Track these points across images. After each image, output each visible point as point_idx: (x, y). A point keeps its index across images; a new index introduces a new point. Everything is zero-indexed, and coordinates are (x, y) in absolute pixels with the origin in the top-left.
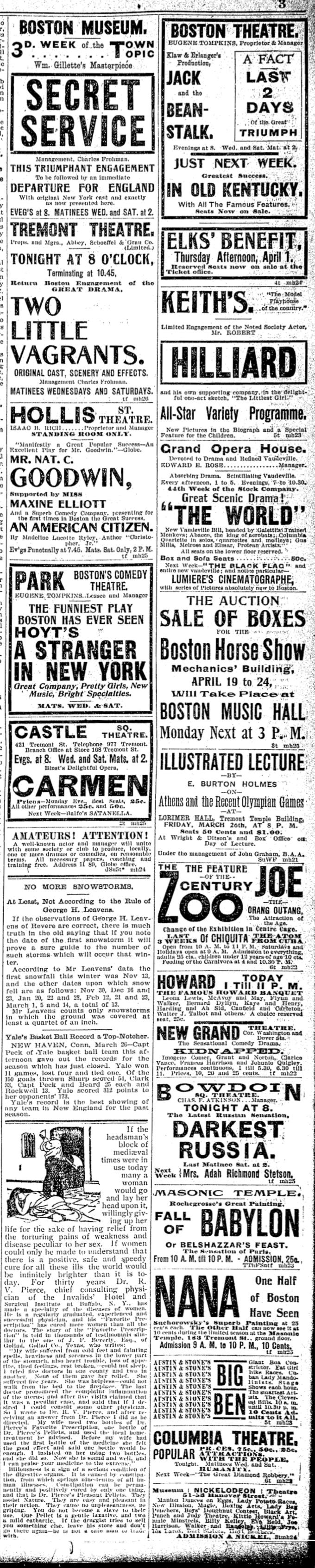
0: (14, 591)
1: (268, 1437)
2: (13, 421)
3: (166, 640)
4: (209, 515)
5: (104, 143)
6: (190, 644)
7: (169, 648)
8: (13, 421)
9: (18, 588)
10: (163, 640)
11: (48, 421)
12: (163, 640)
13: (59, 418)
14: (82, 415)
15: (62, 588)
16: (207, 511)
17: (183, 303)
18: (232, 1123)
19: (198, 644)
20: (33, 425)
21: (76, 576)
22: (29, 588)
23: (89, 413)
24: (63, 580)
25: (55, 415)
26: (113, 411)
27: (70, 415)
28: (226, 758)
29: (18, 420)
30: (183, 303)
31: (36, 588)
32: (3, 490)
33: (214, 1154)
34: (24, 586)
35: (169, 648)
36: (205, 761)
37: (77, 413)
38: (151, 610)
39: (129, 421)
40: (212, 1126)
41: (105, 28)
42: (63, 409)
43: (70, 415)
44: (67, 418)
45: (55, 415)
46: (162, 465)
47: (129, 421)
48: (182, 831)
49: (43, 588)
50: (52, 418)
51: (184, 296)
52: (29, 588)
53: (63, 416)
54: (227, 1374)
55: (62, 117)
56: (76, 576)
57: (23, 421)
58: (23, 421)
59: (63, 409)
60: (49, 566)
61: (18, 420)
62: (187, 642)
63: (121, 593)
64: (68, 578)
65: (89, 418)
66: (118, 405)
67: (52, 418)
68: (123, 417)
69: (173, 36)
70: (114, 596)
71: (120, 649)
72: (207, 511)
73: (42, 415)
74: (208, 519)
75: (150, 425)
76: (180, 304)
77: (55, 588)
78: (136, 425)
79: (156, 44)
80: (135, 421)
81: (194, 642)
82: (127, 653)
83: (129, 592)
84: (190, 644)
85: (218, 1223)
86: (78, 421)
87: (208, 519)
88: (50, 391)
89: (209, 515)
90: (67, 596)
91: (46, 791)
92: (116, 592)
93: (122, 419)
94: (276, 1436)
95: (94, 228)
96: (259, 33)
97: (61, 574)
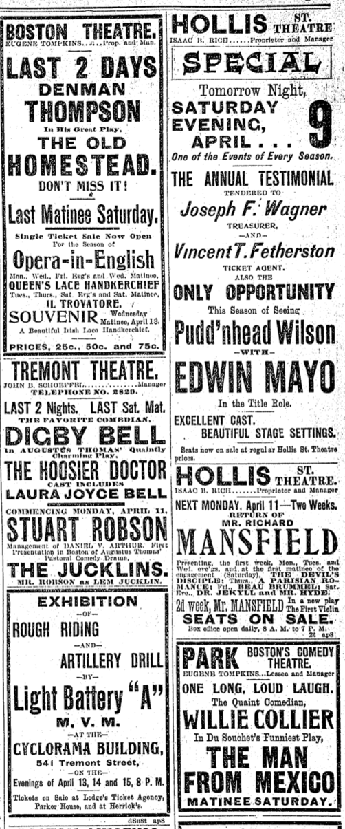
0: (182, 670)
2: (179, 483)
4: (246, 757)
8: (179, 483)
9: (185, 667)
10: (177, 322)
11: (220, 482)
12: (177, 322)
13: (227, 28)
15: (236, 666)
16: (244, 753)
17: (315, 720)
18: (58, 598)
21: (250, 653)
22: (198, 667)
23: (263, 472)
24: (236, 657)
25: (227, 476)
26: (292, 472)
27: (243, 475)
28: (135, 366)
29: (184, 481)
30: (315, 720)
31: (207, 667)
33: (255, 29)
34: (192, 664)
37: (251, 473)
38: (163, 250)
39: (309, 482)
40: (225, 139)
42: (235, 469)
43: (243, 475)
44: (240, 479)
45: (227, 476)
47: (309, 482)
48: (270, 277)
49: (214, 667)
50: (224, 479)
51: (315, 714)
52: (198, 667)
53: (231, 25)
54: (68, 629)
56: (250, 653)
58: (186, 31)
59: (235, 469)
60: (220, 643)
61: (184, 481)
63: (304, 671)
64: (241, 655)
65: (263, 480)
66: (298, 465)
67: (224, 479)
68: (302, 478)
70: (297, 674)
72: (244, 753)
74: (245, 761)
75: (334, 487)
76: (311, 722)
77: (228, 667)
78: (317, 486)
80: (317, 482)
83: (313, 670)
85: (292, 377)
87: (245, 761)
88: (69, 130)
90: (243, 674)
91: (104, 92)
92: (297, 670)
93: (302, 481)
94: (266, 431)
95: (32, 110)
96: (111, 34)
97: (235, 650)
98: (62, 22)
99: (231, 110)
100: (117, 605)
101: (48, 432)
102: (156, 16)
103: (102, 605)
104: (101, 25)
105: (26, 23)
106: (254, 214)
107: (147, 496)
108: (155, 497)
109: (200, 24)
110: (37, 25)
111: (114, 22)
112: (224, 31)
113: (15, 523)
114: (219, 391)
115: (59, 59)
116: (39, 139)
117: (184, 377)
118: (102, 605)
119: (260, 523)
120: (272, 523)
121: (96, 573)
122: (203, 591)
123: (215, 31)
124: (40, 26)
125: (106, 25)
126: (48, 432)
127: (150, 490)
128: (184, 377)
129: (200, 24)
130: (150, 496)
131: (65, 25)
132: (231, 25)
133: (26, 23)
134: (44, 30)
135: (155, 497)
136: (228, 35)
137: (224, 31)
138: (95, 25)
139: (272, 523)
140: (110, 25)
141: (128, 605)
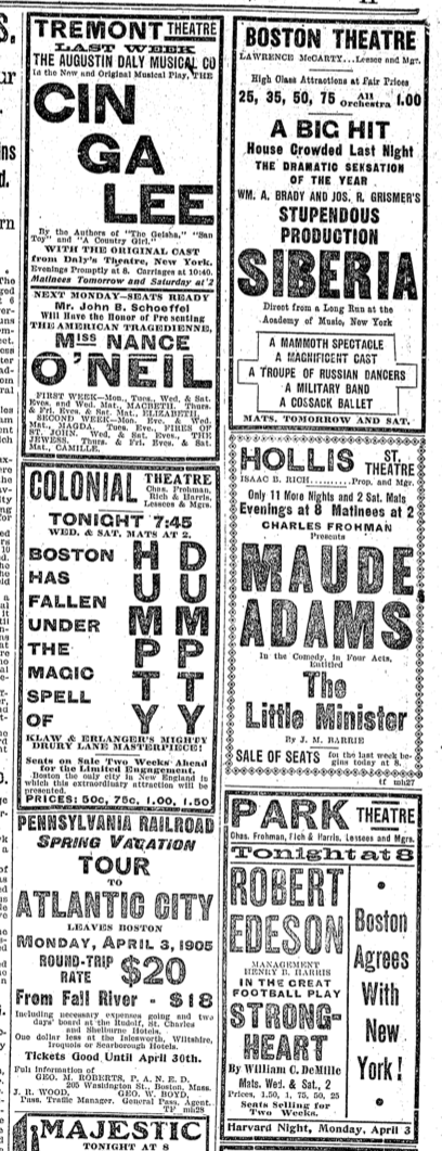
1: (381, 38)
3: (362, 910)
4: (413, 41)
5: (62, 474)
6: (386, 915)
7: (365, 919)
13: (305, 464)
14: (336, 461)
16: (412, 37)
19: (394, 915)
20: (271, 474)
25: (300, 458)
32: (7, 808)
33: (339, 466)
35: (365, 919)
36: (401, 815)
41: (371, 216)
46: (338, 1071)
50: (296, 463)
53: (311, 460)
55: (348, 254)
57: (257, 468)
58: (257, 468)
62: (383, 914)
67: (296, 463)
69: (248, 44)
71: (271, 1047)
72: (412, 37)
73: (282, 459)
74: (412, 44)
79: (17, 282)
81: (390, 914)
82: (310, 894)
84: (386, 915)
86: (331, 469)
87: (412, 44)
89: (413, 41)
96: (367, 43)
98: (314, 27)
99: (58, 33)
100: (72, 515)
101: (172, 340)
102: (213, 468)
103: (77, 559)
104: (354, 32)
105: (270, 26)
106: (153, 1001)
107: (67, 700)
108: (76, 701)
109: (274, 459)
110: (284, 30)
111: (370, 28)
112: (301, 468)
113: (279, 34)
114: (81, 121)
115: (388, 123)
116: (50, 514)
117: (300, 887)
118: (77, 559)
119: (167, 343)
120: (280, 526)
121: (172, 346)
122: (121, 742)
123: (292, 468)
124: (288, 31)
125: (361, 32)
126: (172, 340)
127: (70, 692)
128: (300, 887)
129: (274, 459)
130: (71, 701)
131: (318, 31)
132: (311, 460)
133: (270, 26)
134: (292, 35)
135: (76, 701)
136: (306, 473)
137: (301, 468)
138: (348, 32)
139: (280, 526)
140: (366, 32)
141: (102, 560)
